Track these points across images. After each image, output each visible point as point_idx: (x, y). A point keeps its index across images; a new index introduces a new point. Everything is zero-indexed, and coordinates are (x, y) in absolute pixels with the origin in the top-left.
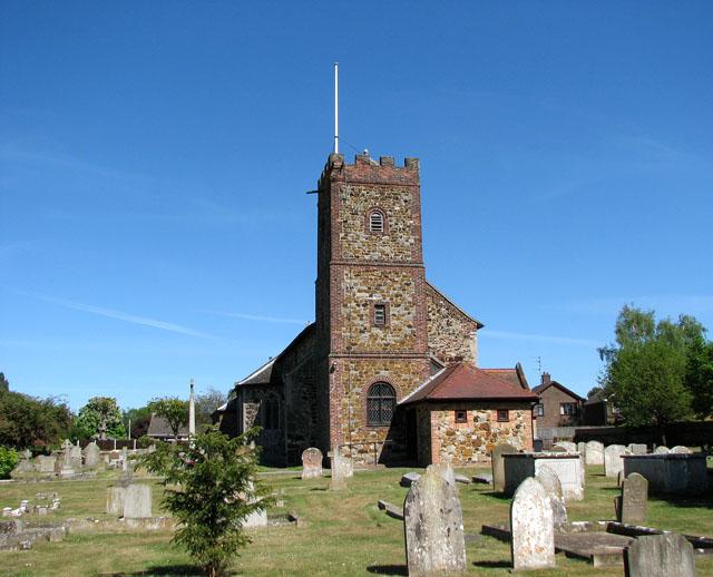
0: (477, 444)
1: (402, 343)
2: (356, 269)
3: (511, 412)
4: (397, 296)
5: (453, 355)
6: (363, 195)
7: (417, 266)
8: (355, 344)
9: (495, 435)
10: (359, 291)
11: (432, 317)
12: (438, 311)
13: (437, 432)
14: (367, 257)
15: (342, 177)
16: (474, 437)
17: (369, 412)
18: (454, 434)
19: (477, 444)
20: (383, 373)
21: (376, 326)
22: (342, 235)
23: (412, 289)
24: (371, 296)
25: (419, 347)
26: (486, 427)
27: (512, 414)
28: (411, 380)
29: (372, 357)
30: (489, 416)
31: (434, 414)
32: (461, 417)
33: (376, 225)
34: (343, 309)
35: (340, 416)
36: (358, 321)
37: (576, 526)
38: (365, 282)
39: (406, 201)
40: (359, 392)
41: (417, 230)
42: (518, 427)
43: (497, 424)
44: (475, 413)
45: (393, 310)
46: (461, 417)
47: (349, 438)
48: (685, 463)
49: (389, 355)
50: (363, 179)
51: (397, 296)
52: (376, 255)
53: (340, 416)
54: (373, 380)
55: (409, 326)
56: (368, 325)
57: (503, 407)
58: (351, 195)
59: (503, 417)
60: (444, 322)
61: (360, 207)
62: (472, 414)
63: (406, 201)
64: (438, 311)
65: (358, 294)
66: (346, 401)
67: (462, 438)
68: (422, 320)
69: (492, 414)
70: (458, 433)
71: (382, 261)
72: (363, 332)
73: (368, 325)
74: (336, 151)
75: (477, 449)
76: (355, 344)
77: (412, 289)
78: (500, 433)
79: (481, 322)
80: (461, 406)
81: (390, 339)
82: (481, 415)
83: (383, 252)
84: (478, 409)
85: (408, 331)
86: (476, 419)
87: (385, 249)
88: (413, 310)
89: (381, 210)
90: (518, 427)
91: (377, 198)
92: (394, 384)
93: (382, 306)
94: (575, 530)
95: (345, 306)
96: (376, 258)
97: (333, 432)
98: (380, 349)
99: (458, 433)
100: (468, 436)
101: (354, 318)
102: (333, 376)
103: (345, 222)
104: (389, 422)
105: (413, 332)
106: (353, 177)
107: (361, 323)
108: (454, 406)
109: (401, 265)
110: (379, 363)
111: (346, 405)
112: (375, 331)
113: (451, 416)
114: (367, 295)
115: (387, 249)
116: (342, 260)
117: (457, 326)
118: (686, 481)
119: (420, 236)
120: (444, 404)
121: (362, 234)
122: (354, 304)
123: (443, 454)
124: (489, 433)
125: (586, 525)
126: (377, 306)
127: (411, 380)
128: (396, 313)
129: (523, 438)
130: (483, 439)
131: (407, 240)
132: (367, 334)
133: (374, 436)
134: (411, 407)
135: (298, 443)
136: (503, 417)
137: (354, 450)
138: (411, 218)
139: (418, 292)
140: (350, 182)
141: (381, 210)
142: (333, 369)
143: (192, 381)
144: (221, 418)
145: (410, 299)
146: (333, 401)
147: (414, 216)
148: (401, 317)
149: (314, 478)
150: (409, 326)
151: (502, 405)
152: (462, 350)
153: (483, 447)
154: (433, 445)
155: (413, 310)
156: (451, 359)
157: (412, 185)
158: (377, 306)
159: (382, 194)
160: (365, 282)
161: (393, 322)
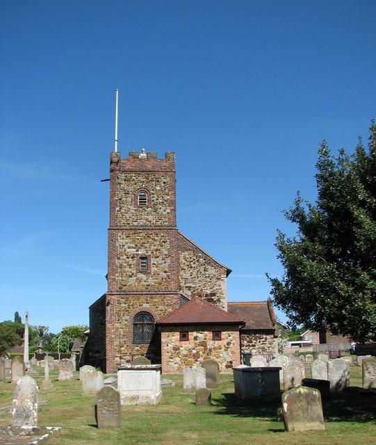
0: (196, 356)
1: (160, 284)
2: (127, 232)
3: (223, 333)
4: (156, 250)
5: (209, 292)
6: (134, 180)
7: (171, 228)
8: (125, 286)
9: (210, 350)
10: (129, 248)
11: (193, 266)
12: (198, 261)
13: (166, 348)
14: (135, 224)
15: (118, 168)
16: (194, 352)
17: (135, 335)
18: (178, 349)
19: (196, 356)
20: (145, 305)
21: (141, 272)
22: (118, 209)
23: (168, 245)
24: (137, 251)
25: (173, 286)
26: (203, 344)
27: (224, 334)
28: (166, 310)
29: (138, 294)
30: (206, 336)
31: (163, 334)
32: (184, 337)
33: (143, 201)
34: (117, 261)
35: (113, 336)
36: (127, 269)
37: (23, 430)
38: (134, 241)
39: (164, 183)
40: (128, 319)
41: (172, 203)
42: (229, 344)
43: (212, 342)
44: (195, 334)
45: (153, 261)
46: (184, 337)
47: (120, 352)
48: (259, 375)
49: (150, 293)
50: (133, 169)
51: (156, 250)
52: (142, 222)
53: (113, 336)
54: (138, 310)
55: (165, 272)
56: (135, 272)
57: (217, 329)
58: (125, 180)
59: (217, 336)
60: (202, 269)
61: (131, 189)
62: (192, 334)
63: (164, 183)
64: (198, 261)
65: (128, 250)
66: (118, 325)
67: (185, 352)
68: (176, 268)
69: (209, 334)
70: (181, 348)
71: (146, 226)
72: (130, 276)
73: (135, 272)
74: (116, 151)
75: (196, 361)
76: (125, 286)
77: (168, 245)
78: (214, 349)
79: (229, 268)
80: (184, 329)
81: (151, 281)
82: (199, 335)
83: (147, 220)
84: (198, 331)
85: (164, 275)
86: (196, 338)
87: (148, 217)
88: (168, 260)
89: (145, 191)
90: (229, 344)
91: (143, 182)
92: (153, 313)
93: (145, 258)
94: (23, 433)
95: (119, 258)
96: (142, 224)
97: (108, 347)
98: (144, 289)
99: (181, 348)
100: (190, 351)
101: (125, 267)
102: (108, 308)
103: (120, 199)
104: (150, 340)
105: (168, 276)
106: (126, 168)
107: (130, 270)
108: (179, 329)
109: (160, 228)
110: (143, 299)
111: (117, 329)
112: (140, 275)
113: (177, 335)
114: (135, 250)
115: (150, 218)
116: (117, 226)
117: (212, 271)
118: (259, 390)
119: (175, 207)
120: (172, 327)
121: (132, 207)
122: (125, 257)
123: (170, 363)
124: (206, 349)
125: (34, 430)
126: (141, 258)
127: (166, 310)
128: (155, 262)
129: (233, 352)
130: (201, 353)
131: (165, 210)
132: (134, 278)
133: (138, 350)
134: (158, 325)
135: (97, 355)
136: (217, 336)
137: (122, 360)
138: (168, 195)
139: (172, 247)
140: (125, 171)
141: (145, 191)
142: (109, 303)
143: (27, 313)
144: (87, 338)
145: (166, 253)
146: (108, 325)
147: (170, 193)
148: (159, 266)
149: (67, 380)
150: (165, 272)
151: (217, 328)
152: (215, 288)
153: (201, 359)
154: (163, 357)
155: (168, 260)
156: (207, 295)
157: (170, 171)
158: (141, 258)
159: (147, 178)
160: (134, 241)
161: (154, 269)
